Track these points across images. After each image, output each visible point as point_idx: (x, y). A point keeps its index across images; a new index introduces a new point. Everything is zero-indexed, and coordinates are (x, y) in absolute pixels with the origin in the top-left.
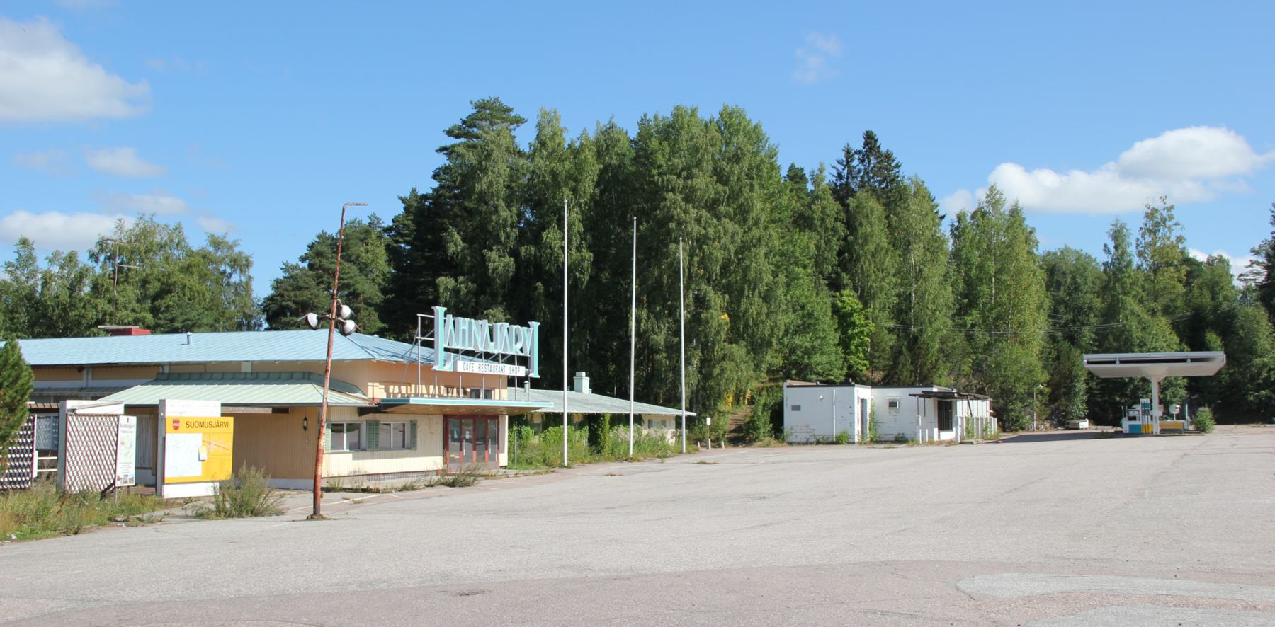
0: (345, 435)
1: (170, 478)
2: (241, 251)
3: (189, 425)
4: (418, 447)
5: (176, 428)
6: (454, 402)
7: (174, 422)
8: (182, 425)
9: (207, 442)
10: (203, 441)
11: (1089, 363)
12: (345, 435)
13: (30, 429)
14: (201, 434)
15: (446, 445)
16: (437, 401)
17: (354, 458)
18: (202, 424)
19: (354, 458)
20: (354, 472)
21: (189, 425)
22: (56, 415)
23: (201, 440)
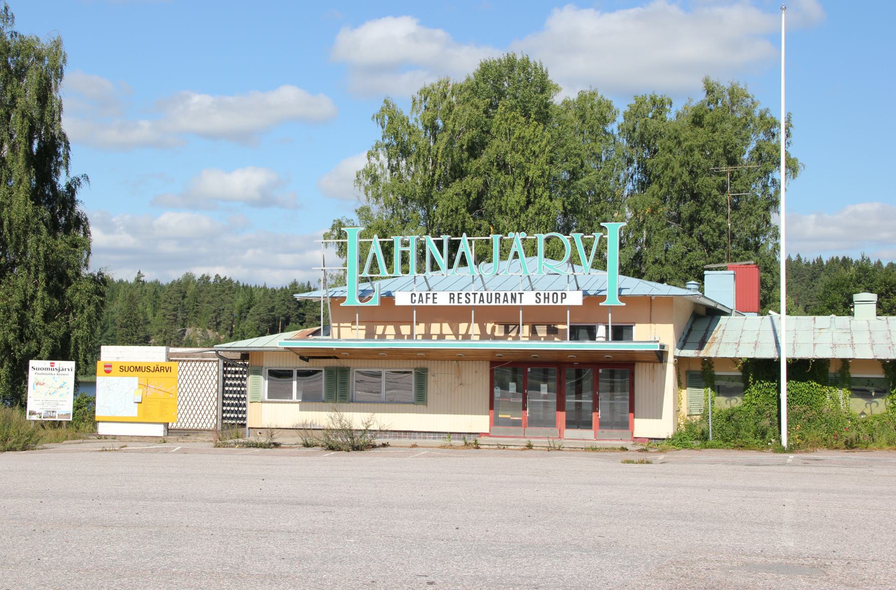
0: (295, 383)
1: (99, 417)
2: (624, 111)
3: (122, 369)
4: (429, 401)
5: (108, 372)
6: (619, 346)
7: (105, 366)
8: (116, 369)
9: (144, 386)
10: (139, 384)
11: (491, 294)
12: (295, 383)
13: (227, 392)
14: (137, 378)
15: (491, 407)
16: (476, 344)
17: (301, 409)
18: (138, 369)
19: (301, 409)
20: (303, 425)
21: (122, 369)
22: (388, 380)
23: (137, 383)
